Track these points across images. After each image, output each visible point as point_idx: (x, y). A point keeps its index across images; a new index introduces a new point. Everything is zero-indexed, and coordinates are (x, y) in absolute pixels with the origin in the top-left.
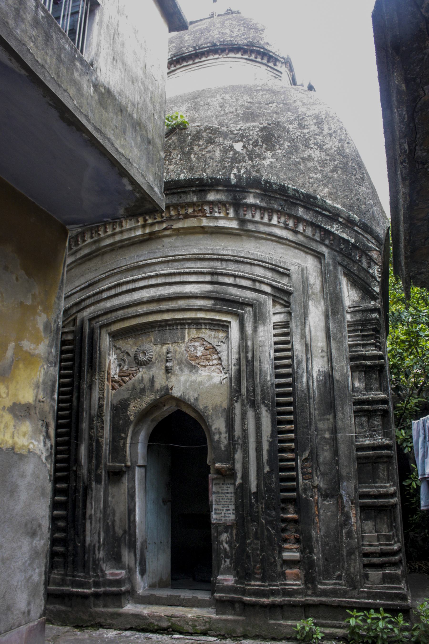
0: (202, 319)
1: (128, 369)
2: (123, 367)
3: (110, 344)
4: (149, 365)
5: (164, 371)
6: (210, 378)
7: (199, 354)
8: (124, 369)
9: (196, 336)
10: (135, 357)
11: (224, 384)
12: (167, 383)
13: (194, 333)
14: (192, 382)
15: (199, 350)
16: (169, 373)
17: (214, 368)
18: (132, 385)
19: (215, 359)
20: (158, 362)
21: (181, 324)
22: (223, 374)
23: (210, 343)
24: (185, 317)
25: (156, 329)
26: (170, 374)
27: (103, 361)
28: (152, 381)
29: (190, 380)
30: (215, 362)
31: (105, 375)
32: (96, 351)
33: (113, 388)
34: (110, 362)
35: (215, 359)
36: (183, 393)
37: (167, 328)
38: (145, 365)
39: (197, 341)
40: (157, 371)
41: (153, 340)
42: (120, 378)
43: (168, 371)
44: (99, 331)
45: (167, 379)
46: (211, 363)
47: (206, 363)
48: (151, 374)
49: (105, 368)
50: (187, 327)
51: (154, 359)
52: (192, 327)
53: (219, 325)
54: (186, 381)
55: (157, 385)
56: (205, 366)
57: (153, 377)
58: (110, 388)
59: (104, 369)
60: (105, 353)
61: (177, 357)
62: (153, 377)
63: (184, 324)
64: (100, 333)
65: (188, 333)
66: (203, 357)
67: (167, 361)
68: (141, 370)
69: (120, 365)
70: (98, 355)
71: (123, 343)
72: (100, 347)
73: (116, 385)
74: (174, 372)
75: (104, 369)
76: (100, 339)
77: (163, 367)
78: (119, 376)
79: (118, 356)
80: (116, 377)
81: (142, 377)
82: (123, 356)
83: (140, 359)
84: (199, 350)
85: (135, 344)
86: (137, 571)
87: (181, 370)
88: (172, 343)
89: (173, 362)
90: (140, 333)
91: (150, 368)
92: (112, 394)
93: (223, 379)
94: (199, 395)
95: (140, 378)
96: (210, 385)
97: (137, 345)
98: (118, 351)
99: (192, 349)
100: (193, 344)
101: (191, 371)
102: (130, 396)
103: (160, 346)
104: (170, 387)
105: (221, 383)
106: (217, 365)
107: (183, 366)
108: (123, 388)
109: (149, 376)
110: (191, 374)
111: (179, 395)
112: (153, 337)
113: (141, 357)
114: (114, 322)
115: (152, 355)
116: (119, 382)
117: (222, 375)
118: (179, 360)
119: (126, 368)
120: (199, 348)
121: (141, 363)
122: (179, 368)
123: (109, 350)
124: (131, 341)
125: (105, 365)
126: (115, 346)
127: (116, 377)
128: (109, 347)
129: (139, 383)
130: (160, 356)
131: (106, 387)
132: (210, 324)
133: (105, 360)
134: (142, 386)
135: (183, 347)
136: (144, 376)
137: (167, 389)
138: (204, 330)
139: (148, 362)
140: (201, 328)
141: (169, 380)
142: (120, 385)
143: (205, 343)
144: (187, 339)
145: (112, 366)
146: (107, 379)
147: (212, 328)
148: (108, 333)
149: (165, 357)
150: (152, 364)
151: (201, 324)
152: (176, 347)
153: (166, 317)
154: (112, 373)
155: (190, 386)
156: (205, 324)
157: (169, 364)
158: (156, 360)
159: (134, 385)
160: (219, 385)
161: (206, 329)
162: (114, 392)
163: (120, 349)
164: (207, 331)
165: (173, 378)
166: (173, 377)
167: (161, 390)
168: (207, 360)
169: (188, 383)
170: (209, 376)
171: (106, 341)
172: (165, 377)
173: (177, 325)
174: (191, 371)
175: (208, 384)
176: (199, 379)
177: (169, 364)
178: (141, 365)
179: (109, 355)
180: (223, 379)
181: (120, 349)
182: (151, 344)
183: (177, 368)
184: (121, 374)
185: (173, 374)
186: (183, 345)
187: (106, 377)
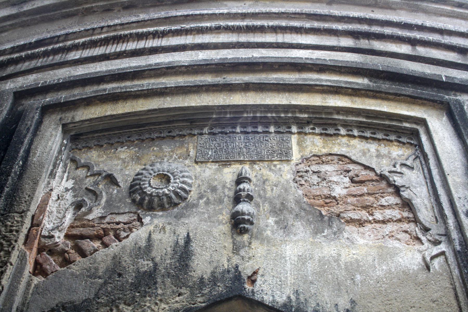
0: (339, 110)
1: (102, 218)
2: (90, 211)
3: (60, 152)
4: (176, 210)
5: (226, 228)
6: (385, 255)
7: (338, 191)
8: (90, 217)
9: (325, 151)
10: (132, 186)
11: (436, 273)
12: (236, 260)
13: (316, 144)
14: (322, 262)
15: (337, 183)
16: (243, 231)
17: (389, 228)
18: (109, 261)
19: (390, 207)
20: (207, 203)
21: (277, 123)
22: (426, 244)
23: (367, 168)
24: (294, 102)
25: (206, 130)
26: (246, 237)
27: (27, 187)
28: (184, 253)
29: (318, 254)
30: (396, 213)
31: (22, 223)
32: (15, 158)
33: (39, 269)
34: (49, 194)
35: (390, 207)
36: (297, 293)
37: (238, 130)
38: (162, 208)
39: (327, 163)
40: (204, 226)
41: (192, 153)
42: (70, 243)
43: (239, 224)
44: (37, 117)
45: (236, 249)
46: (378, 216)
47: (364, 215)
48: (182, 233)
49: (28, 204)
50: (294, 129)
51: (193, 196)
52: (307, 129)
53: (388, 130)
54: (303, 260)
55: (201, 266)
56: (361, 223)
57: (188, 240)
58: (29, 267)
59: (23, 207)
60: (42, 165)
61: (269, 194)
62: (188, 240)
63: (287, 123)
64: (40, 123)
65: (299, 144)
66: (350, 200)
67: (237, 200)
68: (146, 220)
69: (78, 206)
70: (16, 168)
71: (99, 156)
72: (28, 152)
73: (52, 263)
74: (260, 232)
75: (23, 207)
76: (35, 134)
77: (225, 216)
78: (67, 236)
79: (78, 181)
80: (59, 237)
81: (149, 239)
82: (96, 183)
83: (149, 190)
84: (337, 183)
85: (138, 159)
86: (416, 3)
87: (284, 227)
88: (253, 162)
89: (257, 206)
90: (155, 135)
91: (178, 217)
92: (29, 284)
93: (432, 258)
94: (353, 302)
95: (143, 244)
96: (390, 272)
97: (143, 161)
98: (82, 172)
99: (315, 179)
100: (315, 168)
101: (316, 232)
102: (97, 296)
103: (215, 167)
104: (249, 273)
105: (428, 268)
106: (399, 221)
107: (290, 218)
108: (74, 268)
109: (172, 239)
110: (319, 239)
111: (281, 299)
112: (195, 147)
113: (152, 186)
114: (88, 102)
115: (190, 185)
116: (64, 252)
117: (422, 248)
118: (278, 203)
119: (97, 213)
120: (335, 179)
121: (151, 202)
122: (276, 222)
123: (55, 166)
124: (124, 153)
125: (31, 197)
126: (73, 160)
127: (59, 237)
128: (57, 158)
129: (137, 256)
130: (214, 189)
131: (14, 258)
132: (361, 126)
133: (36, 183)
134: (145, 265)
135: (286, 172)
136: (156, 236)
137: (238, 277)
138: (345, 140)
139: (175, 199)
140: (337, 135)
141: (242, 253)
142: (67, 262)
143: (351, 167)
144: (296, 155)
145: (52, 206)
146: (27, 237)
147: (368, 134)
148: (64, 126)
149: (231, 194)
150: (186, 207)
151: (334, 124)
152: (266, 172)
153: (238, 99)
154: (48, 224)
155: (320, 274)
156: (346, 125)
157: (244, 207)
158: (201, 197)
159: (116, 260)
160: (423, 276)
161: (354, 137)
162: (36, 280)
163: (87, 167)
164: (355, 142)
165: (258, 250)
166: (255, 244)
167: (214, 280)
168: (365, 207)
169: (310, 267)
170: (380, 247)
171: (51, 141)
172: (229, 244)
173: (266, 123)
174: (316, 232)
175: (380, 271)
176: (348, 255)
177: (244, 207)
178: (151, 208)
179: (52, 175)
180: (432, 258)
181: (87, 167)
182: (187, 162)
183: (271, 221)
184: (75, 232)
185: (259, 236)
186: (286, 168)
187: (24, 231)
